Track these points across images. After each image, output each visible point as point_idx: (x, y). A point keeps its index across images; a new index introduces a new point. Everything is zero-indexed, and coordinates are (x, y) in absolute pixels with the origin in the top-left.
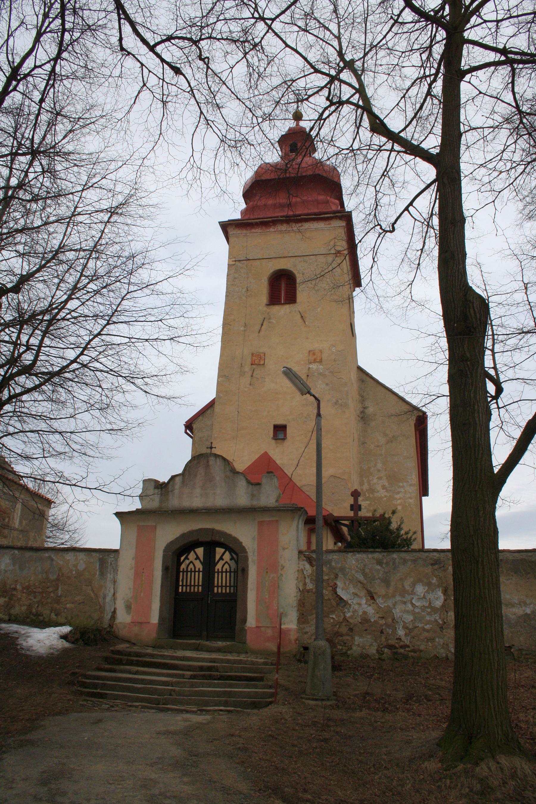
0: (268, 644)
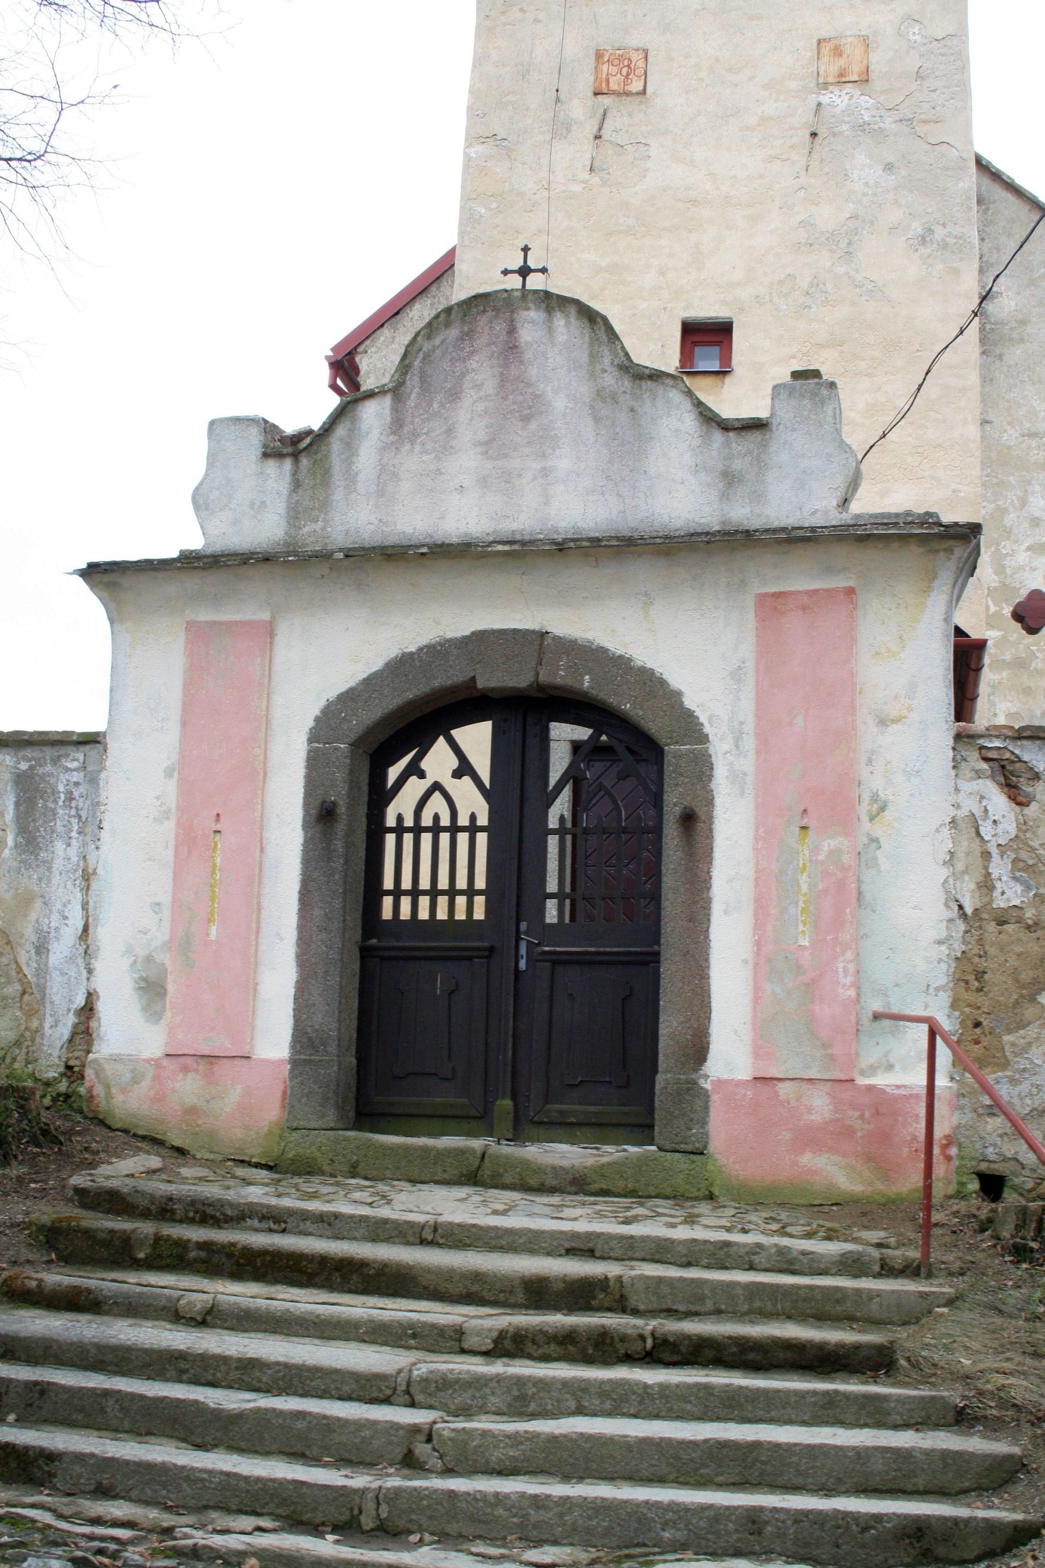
0: (807, 1159)
